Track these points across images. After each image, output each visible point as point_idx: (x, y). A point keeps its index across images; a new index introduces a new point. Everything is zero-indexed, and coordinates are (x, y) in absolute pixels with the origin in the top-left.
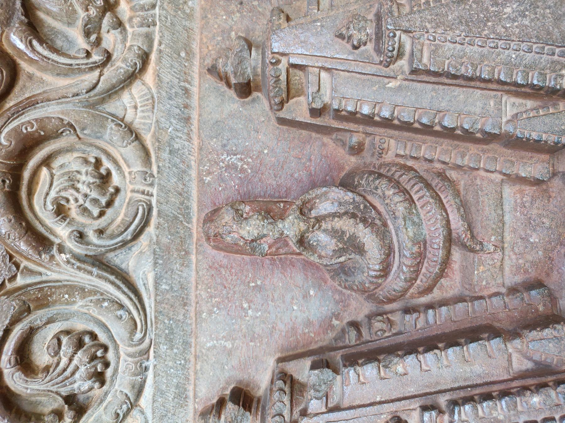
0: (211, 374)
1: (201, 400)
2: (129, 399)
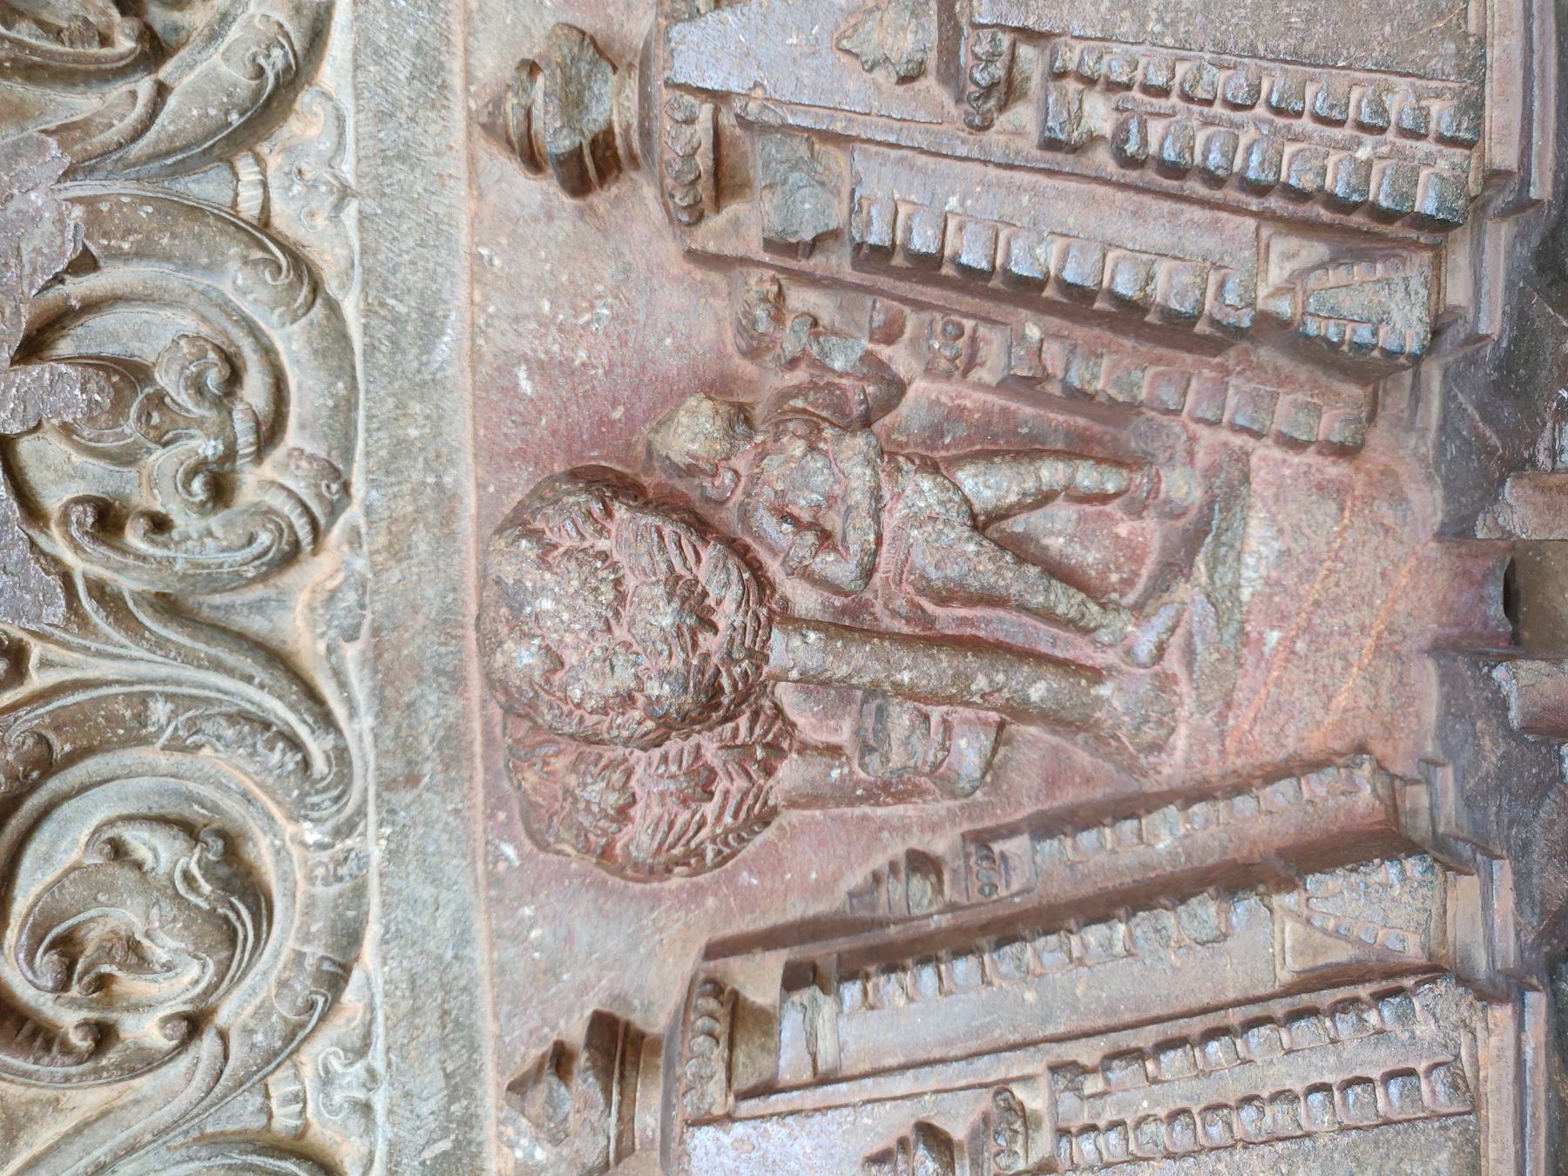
0: (508, 21)
1: (484, 86)
2: (287, 36)
